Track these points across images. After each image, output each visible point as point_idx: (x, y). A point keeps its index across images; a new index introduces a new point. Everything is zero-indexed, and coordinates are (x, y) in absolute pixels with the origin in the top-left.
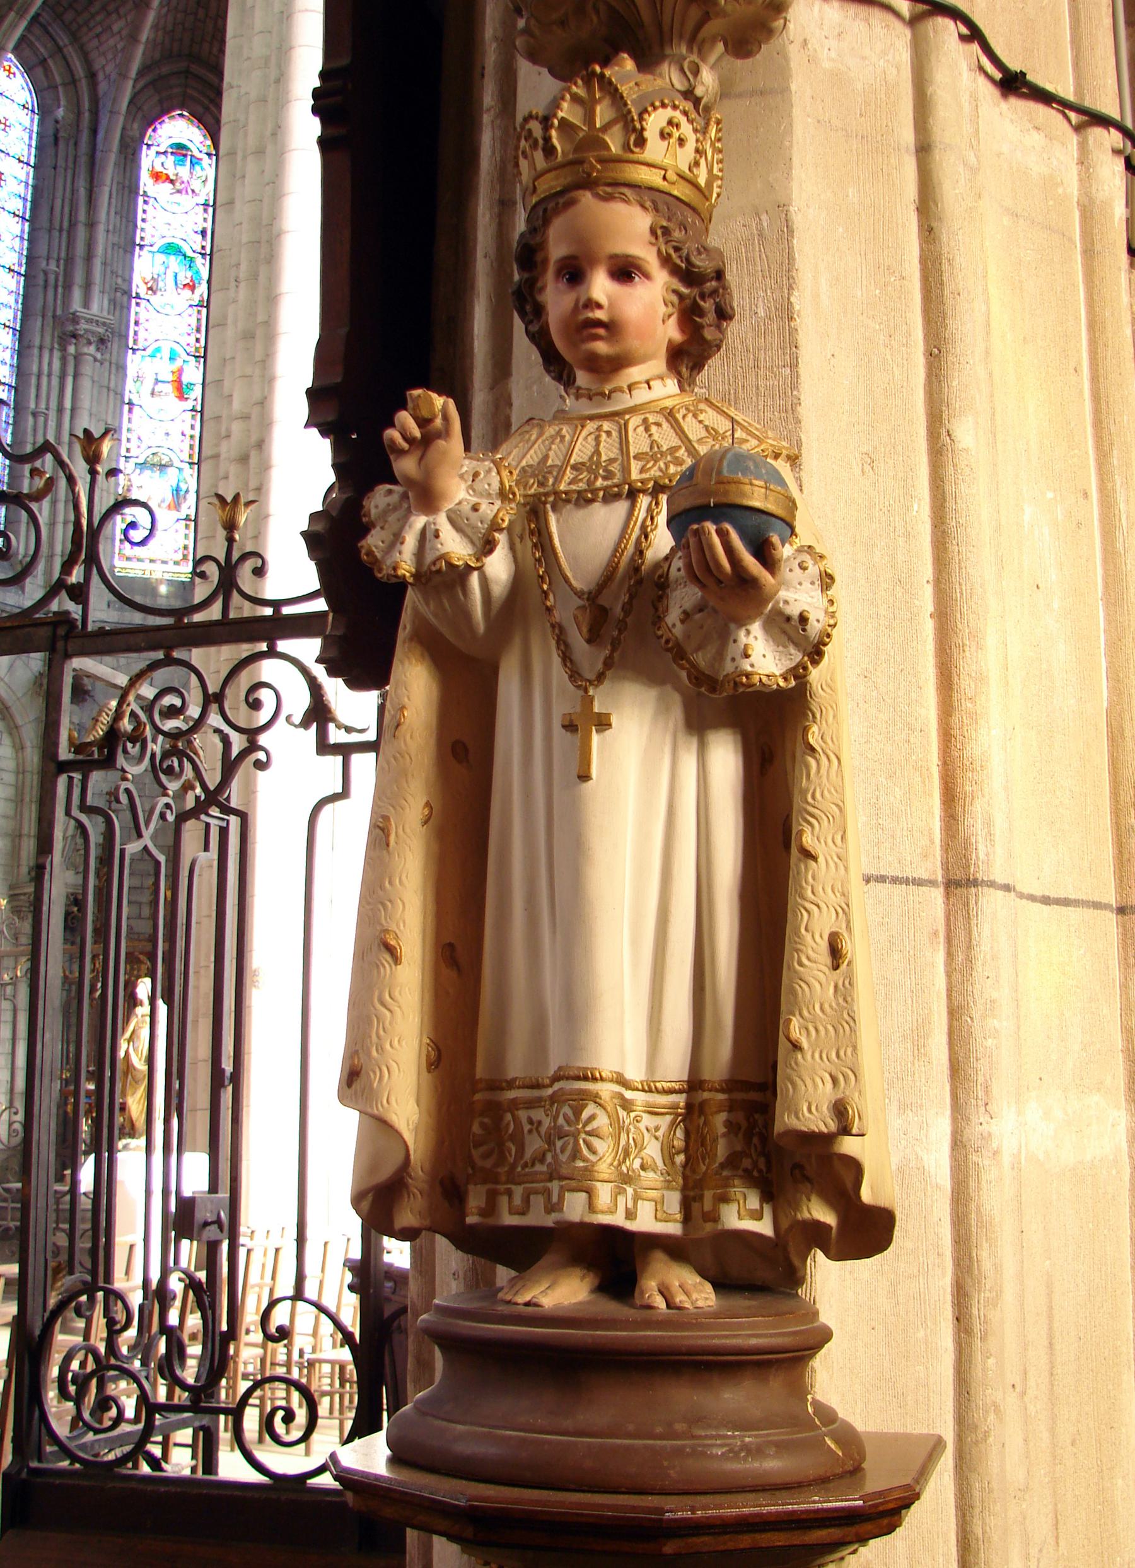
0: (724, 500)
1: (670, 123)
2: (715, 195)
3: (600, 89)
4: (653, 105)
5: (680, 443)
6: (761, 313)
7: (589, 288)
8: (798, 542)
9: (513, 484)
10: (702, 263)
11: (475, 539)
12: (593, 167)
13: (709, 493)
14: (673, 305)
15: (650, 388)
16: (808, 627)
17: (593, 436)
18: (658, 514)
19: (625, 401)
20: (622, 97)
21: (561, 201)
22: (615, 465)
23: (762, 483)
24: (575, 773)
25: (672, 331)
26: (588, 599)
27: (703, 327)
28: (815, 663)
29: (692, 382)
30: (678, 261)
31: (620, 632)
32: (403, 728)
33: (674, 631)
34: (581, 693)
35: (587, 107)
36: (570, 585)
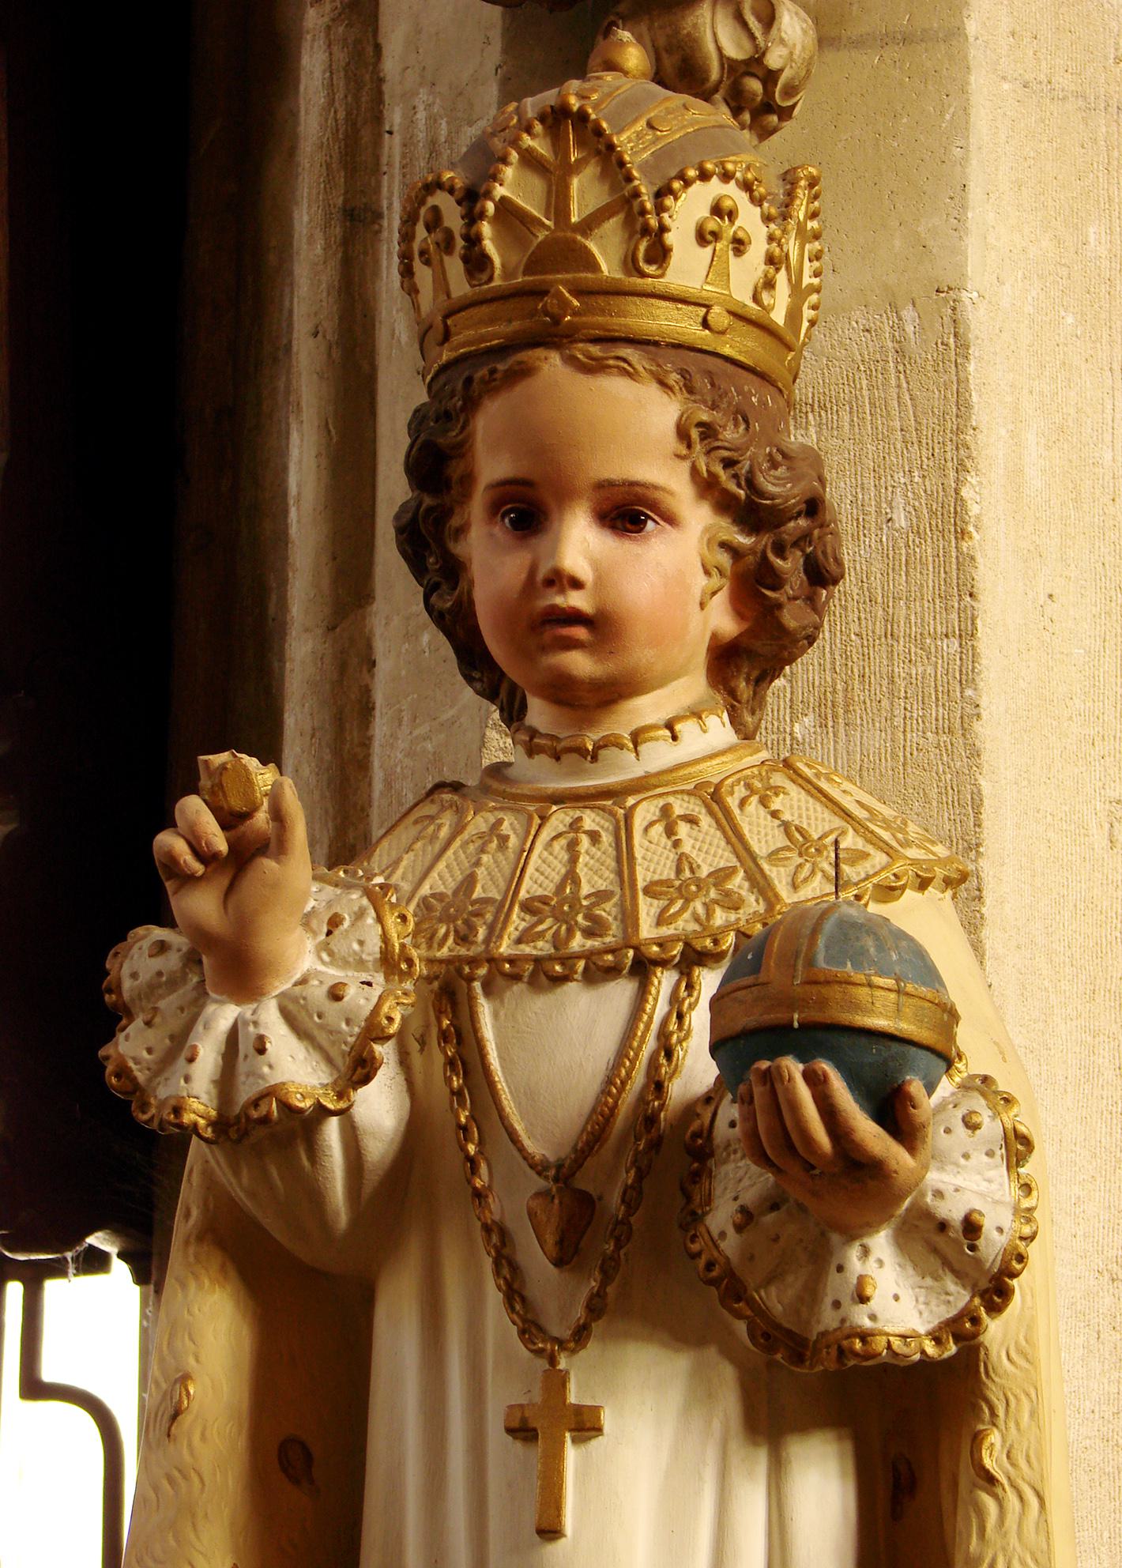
0: (817, 1016)
1: (717, 210)
2: (805, 324)
3: (581, 143)
4: (681, 176)
5: (734, 862)
6: (901, 520)
8: (962, 1070)
9: (408, 941)
10: (776, 486)
11: (334, 1053)
12: (565, 304)
13: (791, 1003)
14: (721, 573)
15: (674, 738)
16: (981, 1243)
17: (563, 842)
18: (692, 1007)
19: (624, 767)
20: (622, 164)
22: (608, 906)
23: (890, 982)
24: (529, 1530)
26: (556, 1180)
27: (779, 606)
28: (995, 1309)
30: (732, 487)
31: (618, 1247)
32: (186, 1420)
33: (723, 1245)
34: (543, 1364)
36: (521, 1149)
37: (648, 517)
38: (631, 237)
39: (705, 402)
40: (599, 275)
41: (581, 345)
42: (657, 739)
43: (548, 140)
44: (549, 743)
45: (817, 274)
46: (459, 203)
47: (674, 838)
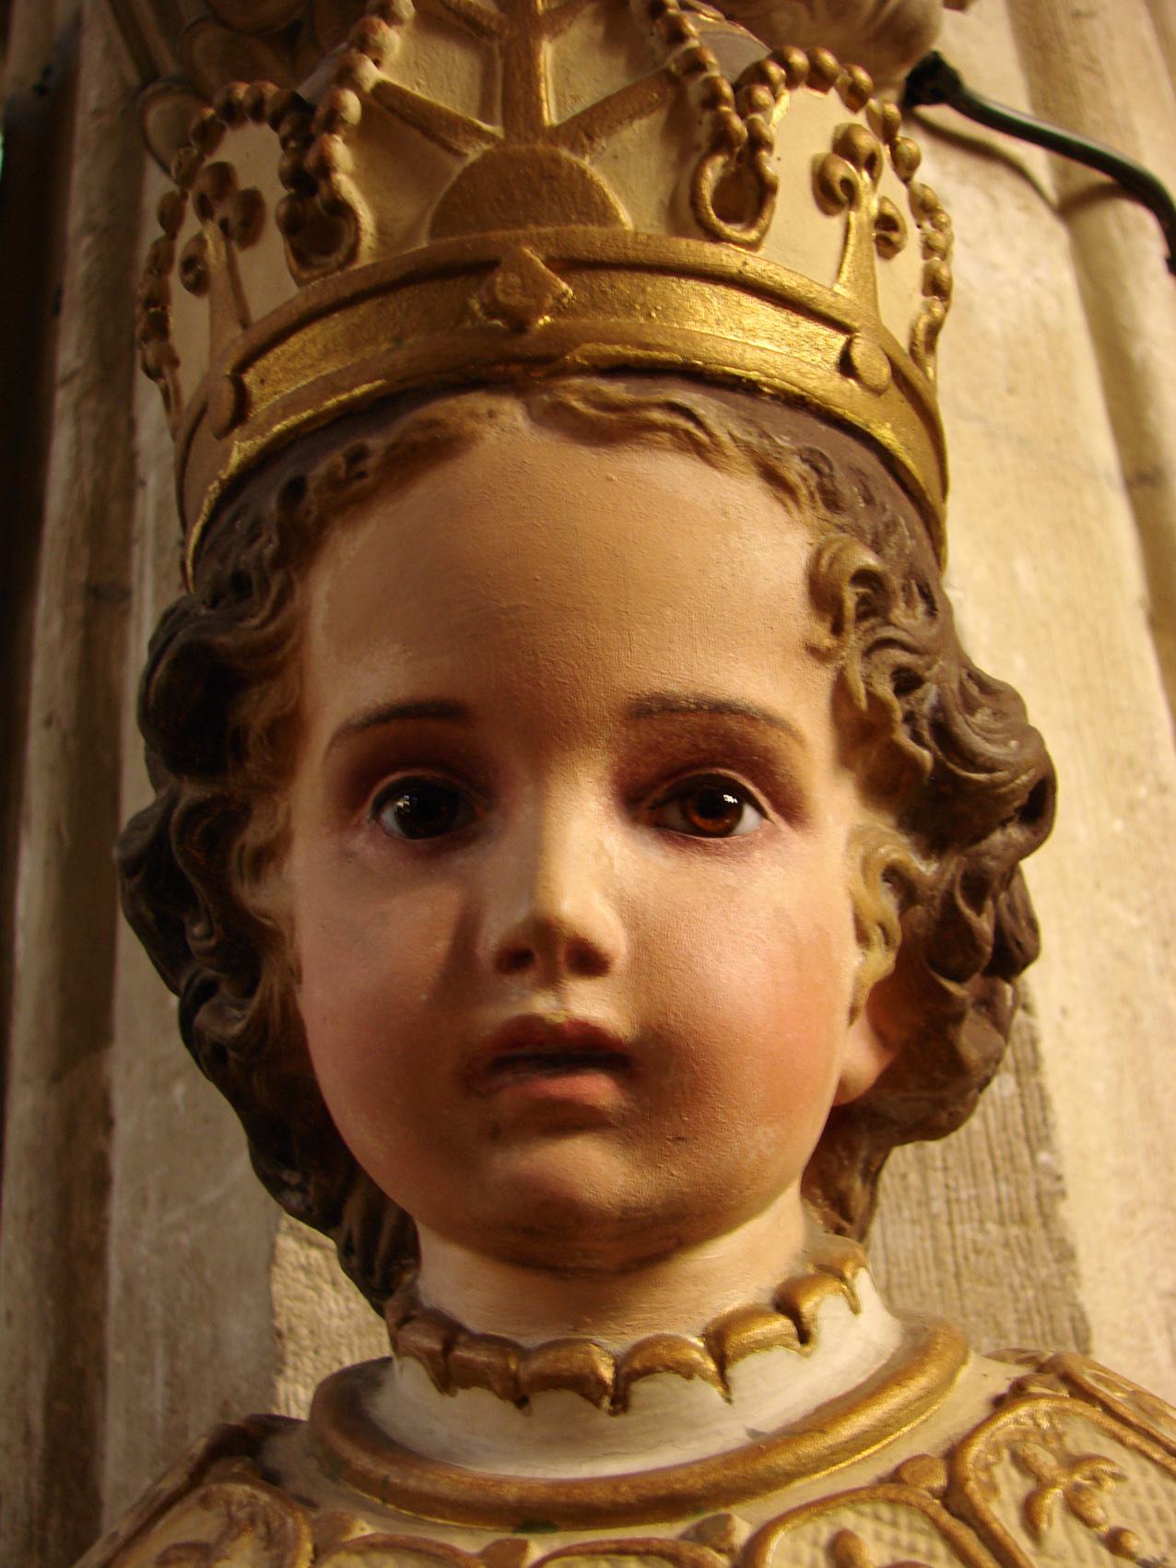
19: (698, 1429)
21: (376, 443)
37: (745, 797)
38: (683, 158)
39: (859, 533)
41: (577, 382)
44: (496, 1361)
46: (275, 126)
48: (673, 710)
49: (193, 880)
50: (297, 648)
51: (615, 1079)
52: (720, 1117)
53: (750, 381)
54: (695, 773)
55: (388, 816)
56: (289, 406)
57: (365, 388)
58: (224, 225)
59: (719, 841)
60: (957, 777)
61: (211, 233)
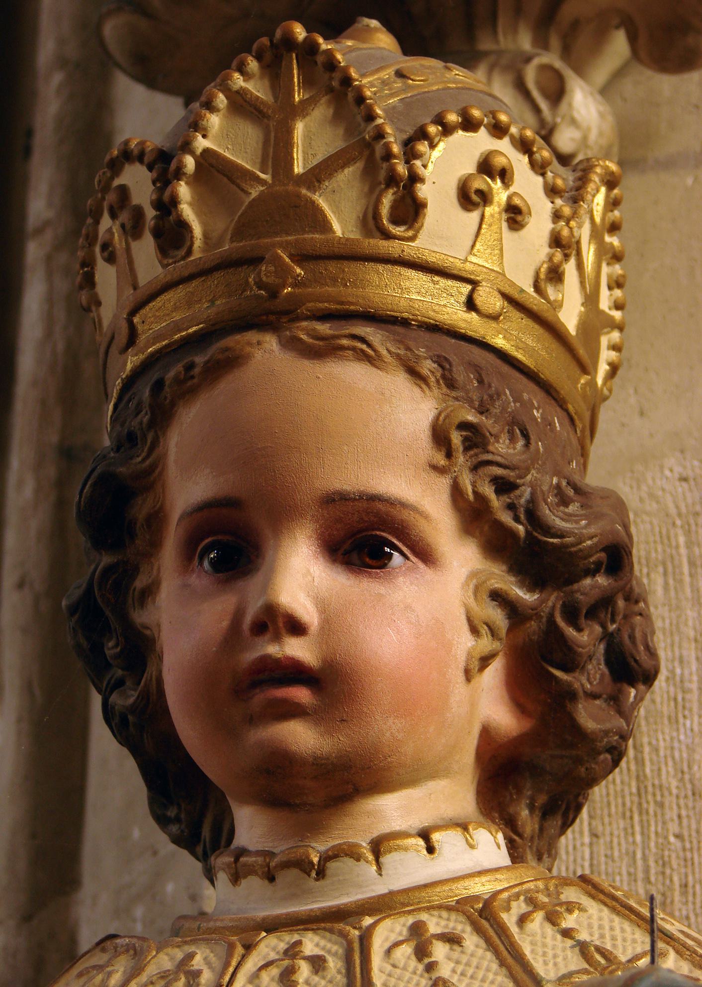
1: (486, 167)
2: (603, 369)
3: (308, 82)
4: (439, 120)
7: (267, 584)
10: (568, 523)
12: (283, 271)
14: (493, 632)
15: (431, 850)
17: (275, 971)
20: (360, 99)
21: (200, 359)
25: (488, 704)
27: (571, 695)
29: (545, 851)
30: (506, 518)
35: (271, 123)
38: (371, 190)
39: (470, 401)
40: (330, 236)
41: (304, 324)
42: (406, 849)
43: (266, 82)
45: (618, 306)
46: (150, 168)
47: (427, 961)
48: (346, 500)
49: (108, 613)
50: (161, 474)
51: (311, 690)
52: (365, 710)
53: (402, 318)
54: (364, 534)
55: (206, 564)
56: (158, 338)
57: (194, 329)
58: (123, 226)
59: (378, 571)
60: (539, 541)
61: (116, 230)
